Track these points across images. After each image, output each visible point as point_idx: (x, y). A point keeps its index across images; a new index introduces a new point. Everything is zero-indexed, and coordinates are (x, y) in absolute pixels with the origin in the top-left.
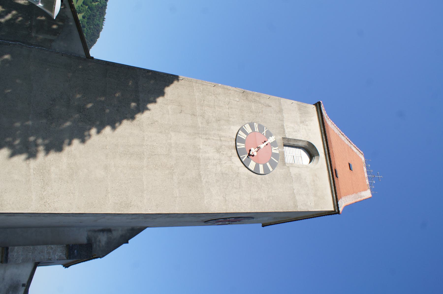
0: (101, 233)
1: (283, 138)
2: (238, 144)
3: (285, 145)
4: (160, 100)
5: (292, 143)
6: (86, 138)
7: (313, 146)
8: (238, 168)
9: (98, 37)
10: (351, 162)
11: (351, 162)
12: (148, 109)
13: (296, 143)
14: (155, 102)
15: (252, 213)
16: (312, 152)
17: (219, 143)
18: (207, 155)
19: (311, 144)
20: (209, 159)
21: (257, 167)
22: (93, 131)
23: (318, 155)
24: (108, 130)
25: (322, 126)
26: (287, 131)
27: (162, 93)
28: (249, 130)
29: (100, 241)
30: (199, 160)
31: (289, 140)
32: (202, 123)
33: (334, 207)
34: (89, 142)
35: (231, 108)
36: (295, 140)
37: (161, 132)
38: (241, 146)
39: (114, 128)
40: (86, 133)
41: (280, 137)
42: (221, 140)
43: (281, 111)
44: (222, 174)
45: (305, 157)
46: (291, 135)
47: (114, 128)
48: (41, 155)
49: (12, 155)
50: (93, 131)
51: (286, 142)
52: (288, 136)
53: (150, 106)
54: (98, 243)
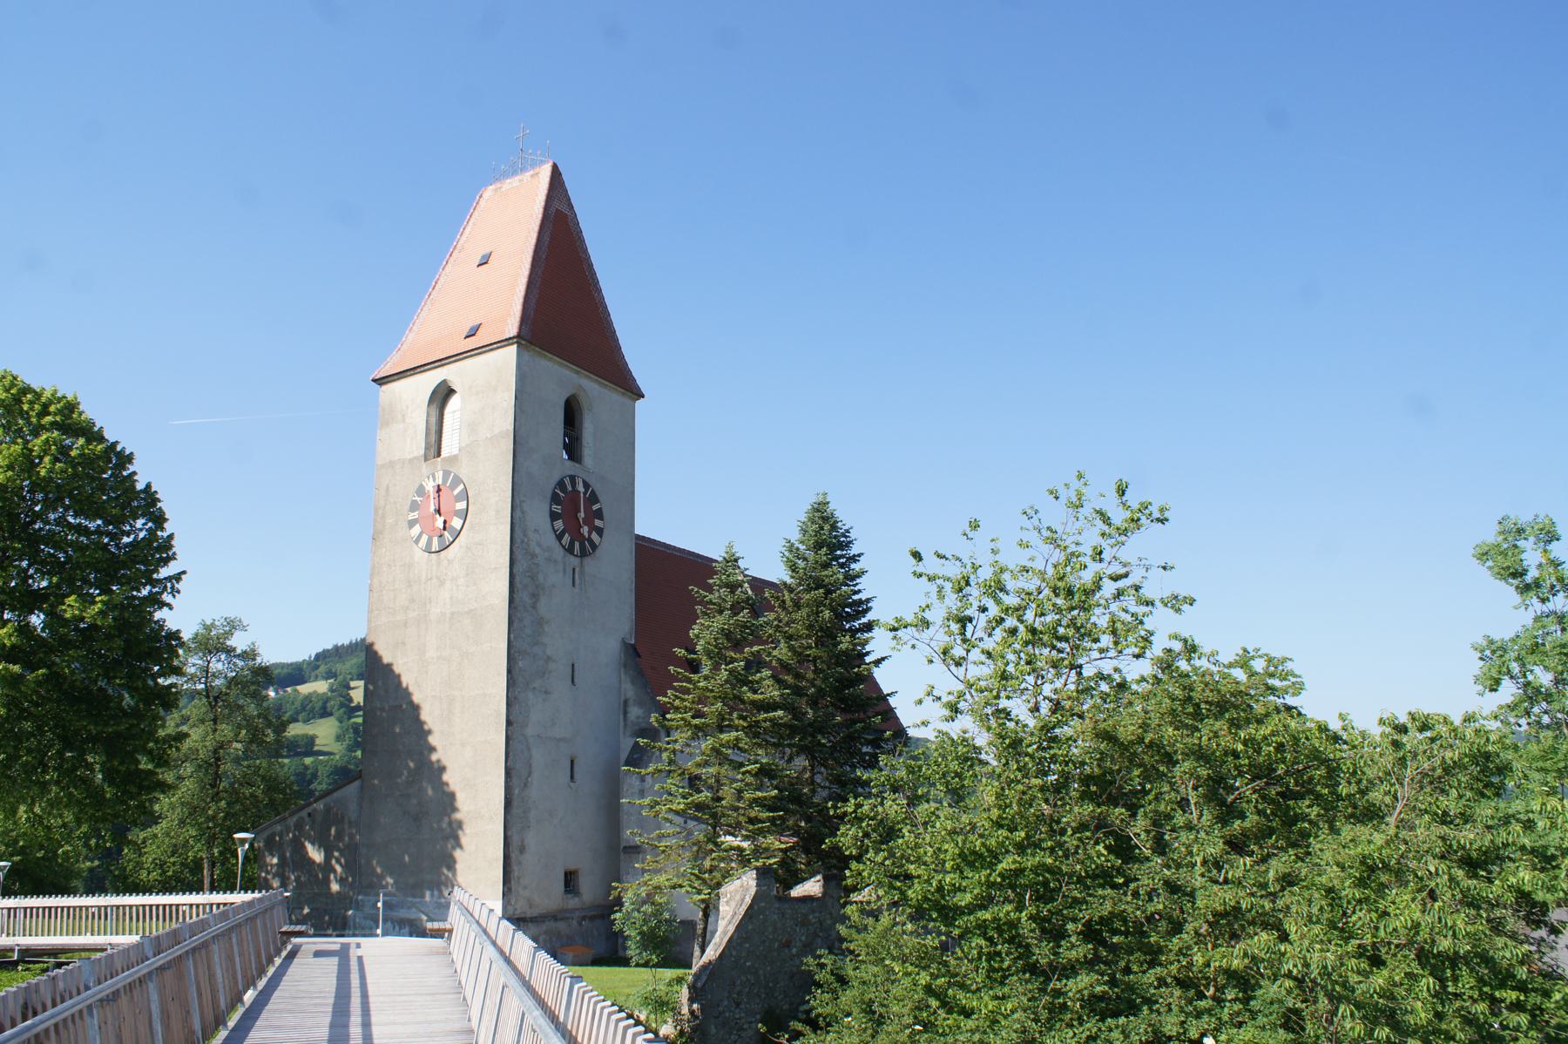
0: (629, 715)
1: (426, 460)
3: (439, 455)
4: (397, 669)
5: (433, 438)
6: (441, 765)
7: (434, 393)
8: (461, 547)
10: (275, 1011)
11: (275, 1011)
12: (407, 688)
13: (434, 428)
14: (399, 676)
15: (518, 514)
16: (443, 391)
17: (434, 581)
19: (431, 398)
20: (451, 598)
21: (457, 513)
22: (434, 757)
23: (445, 381)
24: (433, 740)
25: (405, 374)
26: (416, 454)
27: (389, 666)
28: (417, 530)
29: (638, 717)
30: (453, 614)
32: (414, 610)
33: (512, 344)
34: (445, 762)
35: (394, 561)
36: (427, 434)
37: (427, 673)
38: (435, 546)
39: (429, 732)
40: (436, 766)
41: (425, 468)
42: (431, 579)
43: (392, 464)
44: (467, 574)
45: (454, 404)
48: (458, 816)
49: (460, 846)
50: (434, 757)
51: (433, 451)
52: (422, 452)
53: (404, 685)
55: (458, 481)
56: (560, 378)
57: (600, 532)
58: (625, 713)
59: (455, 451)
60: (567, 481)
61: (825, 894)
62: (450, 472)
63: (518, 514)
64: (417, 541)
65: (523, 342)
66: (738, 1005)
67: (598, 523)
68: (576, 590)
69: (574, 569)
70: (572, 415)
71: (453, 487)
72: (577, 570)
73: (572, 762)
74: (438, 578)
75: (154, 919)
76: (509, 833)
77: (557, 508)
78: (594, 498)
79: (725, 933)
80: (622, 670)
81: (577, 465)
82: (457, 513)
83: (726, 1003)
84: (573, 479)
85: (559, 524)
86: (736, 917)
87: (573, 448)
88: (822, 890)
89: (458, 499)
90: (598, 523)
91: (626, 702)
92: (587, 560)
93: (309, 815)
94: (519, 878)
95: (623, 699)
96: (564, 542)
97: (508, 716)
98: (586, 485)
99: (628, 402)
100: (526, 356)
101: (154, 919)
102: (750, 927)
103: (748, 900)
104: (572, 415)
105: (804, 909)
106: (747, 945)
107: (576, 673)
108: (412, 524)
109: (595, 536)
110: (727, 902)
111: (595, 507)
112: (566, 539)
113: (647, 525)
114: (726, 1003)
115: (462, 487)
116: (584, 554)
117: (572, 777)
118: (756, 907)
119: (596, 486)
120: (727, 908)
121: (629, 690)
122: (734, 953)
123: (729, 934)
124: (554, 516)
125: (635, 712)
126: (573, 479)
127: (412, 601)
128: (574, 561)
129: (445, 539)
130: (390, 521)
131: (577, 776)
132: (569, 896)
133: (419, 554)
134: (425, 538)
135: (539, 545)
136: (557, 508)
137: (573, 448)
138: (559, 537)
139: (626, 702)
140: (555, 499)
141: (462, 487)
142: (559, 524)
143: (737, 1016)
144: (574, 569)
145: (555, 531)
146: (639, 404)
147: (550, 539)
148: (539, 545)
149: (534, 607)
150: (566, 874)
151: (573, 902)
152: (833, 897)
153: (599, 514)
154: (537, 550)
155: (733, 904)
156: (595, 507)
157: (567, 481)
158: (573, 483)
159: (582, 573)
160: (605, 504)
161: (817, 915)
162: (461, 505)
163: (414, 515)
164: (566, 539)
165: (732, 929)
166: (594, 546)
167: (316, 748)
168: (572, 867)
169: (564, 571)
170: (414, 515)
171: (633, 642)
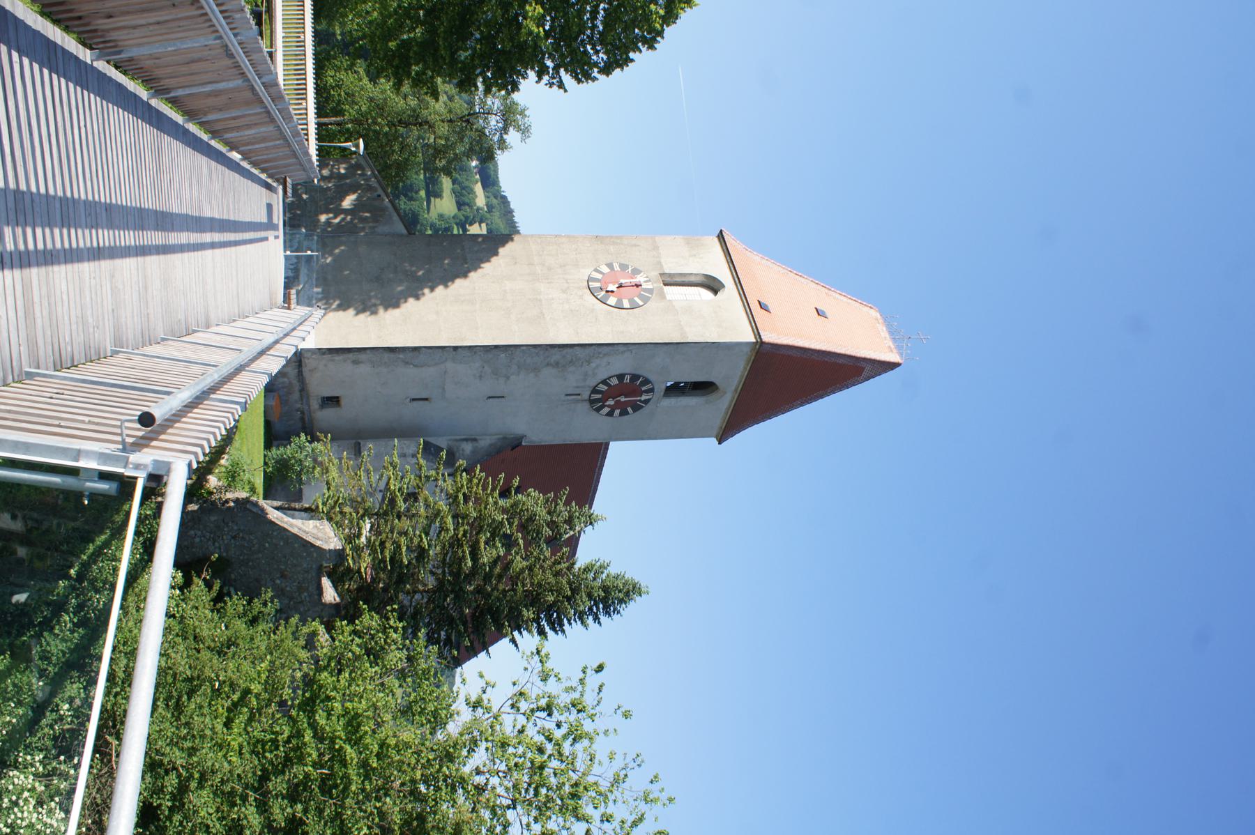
0: (465, 442)
1: (661, 274)
2: (590, 283)
3: (665, 285)
4: (494, 259)
5: (678, 279)
8: (593, 305)
9: (465, 275)
12: (480, 268)
18: (550, 296)
21: (620, 301)
22: (426, 291)
23: (723, 286)
28: (605, 270)
29: (463, 450)
31: (670, 275)
33: (756, 338)
34: (423, 299)
37: (493, 282)
39: (446, 286)
41: (654, 274)
42: (567, 283)
43: (656, 248)
44: (572, 311)
45: (706, 294)
46: (671, 267)
47: (446, 286)
49: (357, 314)
51: (668, 280)
54: (461, 452)
55: (646, 300)
56: (731, 378)
57: (610, 414)
58: (466, 440)
59: (668, 297)
60: (649, 386)
61: (325, 605)
62: (652, 294)
63: (622, 349)
64: (596, 270)
65: (757, 347)
66: (234, 537)
67: (617, 412)
68: (563, 397)
69: (579, 395)
70: (703, 388)
71: (640, 296)
72: (579, 397)
73: (426, 399)
74: (568, 288)
75: (297, 102)
76: (368, 351)
77: (627, 379)
78: (636, 408)
79: (292, 525)
80: (501, 436)
81: (662, 393)
82: (620, 301)
83: (235, 528)
84: (651, 390)
85: (614, 381)
86: (304, 534)
87: (675, 390)
88: (328, 602)
89: (631, 301)
90: (617, 412)
91: (475, 440)
92: (587, 405)
93: (379, 196)
94: (333, 360)
95: (477, 437)
96: (601, 385)
97: (461, 347)
98: (646, 402)
99: (715, 433)
100: (746, 350)
101: (297, 102)
102: (296, 545)
103: (318, 543)
104: (703, 388)
105: (312, 589)
106: (282, 544)
107: (497, 399)
108: (610, 266)
109: (606, 410)
110: (316, 526)
111: (629, 409)
112: (603, 388)
113: (614, 447)
114: (235, 528)
115: (641, 303)
116: (592, 402)
117: (414, 400)
118: (312, 549)
119: (647, 409)
120: (311, 526)
121: (485, 442)
122: (275, 533)
123: (290, 529)
124: (621, 377)
125: (468, 448)
126: (651, 390)
127: (549, 269)
128: (586, 395)
129: (599, 292)
130: (612, 248)
131: (415, 403)
132: (320, 401)
133: (586, 272)
134: (599, 276)
135: (597, 367)
136: (627, 379)
137: (675, 390)
138: (604, 382)
139: (475, 440)
140: (635, 377)
141: (641, 303)
142: (614, 381)
143: (225, 537)
144: (579, 395)
145: (609, 378)
146: (714, 441)
147: (603, 375)
148: (597, 367)
149: (548, 365)
150: (338, 397)
151: (315, 404)
152: (322, 611)
153: (624, 413)
154: (593, 365)
155: (315, 531)
156: (629, 409)
157: (649, 386)
158: (647, 391)
159: (578, 401)
160: (633, 417)
161: (308, 599)
162: (626, 304)
163: (617, 268)
164: (603, 388)
165: (295, 531)
166: (598, 410)
167: (432, 199)
168: (343, 402)
169: (577, 387)
170: (617, 268)
171: (523, 444)
